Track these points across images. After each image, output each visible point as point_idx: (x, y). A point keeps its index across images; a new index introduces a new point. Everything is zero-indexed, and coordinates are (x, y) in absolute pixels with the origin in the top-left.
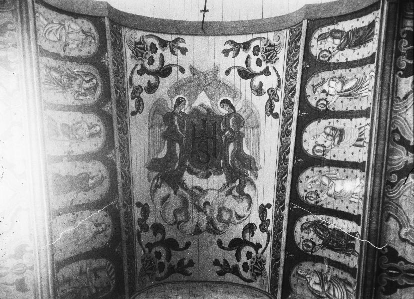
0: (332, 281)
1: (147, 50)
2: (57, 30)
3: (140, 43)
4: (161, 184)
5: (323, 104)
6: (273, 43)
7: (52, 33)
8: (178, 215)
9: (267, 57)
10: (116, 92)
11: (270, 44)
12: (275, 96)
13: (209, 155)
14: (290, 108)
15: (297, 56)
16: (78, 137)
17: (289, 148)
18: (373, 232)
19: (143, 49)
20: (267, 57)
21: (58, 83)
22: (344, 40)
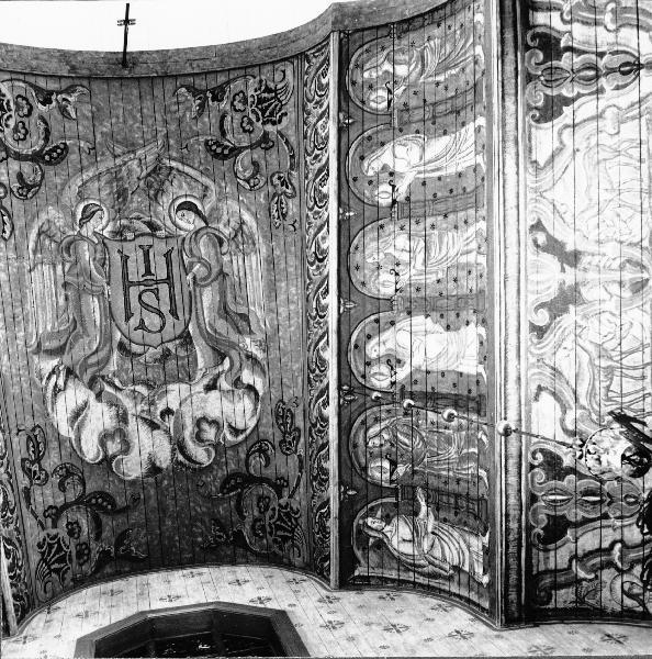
0: (437, 532)
1: (10, 110)
4: (65, 384)
6: (272, 85)
8: (109, 443)
9: (264, 112)
14: (320, 207)
17: (327, 285)
20: (264, 112)
22: (416, 66)
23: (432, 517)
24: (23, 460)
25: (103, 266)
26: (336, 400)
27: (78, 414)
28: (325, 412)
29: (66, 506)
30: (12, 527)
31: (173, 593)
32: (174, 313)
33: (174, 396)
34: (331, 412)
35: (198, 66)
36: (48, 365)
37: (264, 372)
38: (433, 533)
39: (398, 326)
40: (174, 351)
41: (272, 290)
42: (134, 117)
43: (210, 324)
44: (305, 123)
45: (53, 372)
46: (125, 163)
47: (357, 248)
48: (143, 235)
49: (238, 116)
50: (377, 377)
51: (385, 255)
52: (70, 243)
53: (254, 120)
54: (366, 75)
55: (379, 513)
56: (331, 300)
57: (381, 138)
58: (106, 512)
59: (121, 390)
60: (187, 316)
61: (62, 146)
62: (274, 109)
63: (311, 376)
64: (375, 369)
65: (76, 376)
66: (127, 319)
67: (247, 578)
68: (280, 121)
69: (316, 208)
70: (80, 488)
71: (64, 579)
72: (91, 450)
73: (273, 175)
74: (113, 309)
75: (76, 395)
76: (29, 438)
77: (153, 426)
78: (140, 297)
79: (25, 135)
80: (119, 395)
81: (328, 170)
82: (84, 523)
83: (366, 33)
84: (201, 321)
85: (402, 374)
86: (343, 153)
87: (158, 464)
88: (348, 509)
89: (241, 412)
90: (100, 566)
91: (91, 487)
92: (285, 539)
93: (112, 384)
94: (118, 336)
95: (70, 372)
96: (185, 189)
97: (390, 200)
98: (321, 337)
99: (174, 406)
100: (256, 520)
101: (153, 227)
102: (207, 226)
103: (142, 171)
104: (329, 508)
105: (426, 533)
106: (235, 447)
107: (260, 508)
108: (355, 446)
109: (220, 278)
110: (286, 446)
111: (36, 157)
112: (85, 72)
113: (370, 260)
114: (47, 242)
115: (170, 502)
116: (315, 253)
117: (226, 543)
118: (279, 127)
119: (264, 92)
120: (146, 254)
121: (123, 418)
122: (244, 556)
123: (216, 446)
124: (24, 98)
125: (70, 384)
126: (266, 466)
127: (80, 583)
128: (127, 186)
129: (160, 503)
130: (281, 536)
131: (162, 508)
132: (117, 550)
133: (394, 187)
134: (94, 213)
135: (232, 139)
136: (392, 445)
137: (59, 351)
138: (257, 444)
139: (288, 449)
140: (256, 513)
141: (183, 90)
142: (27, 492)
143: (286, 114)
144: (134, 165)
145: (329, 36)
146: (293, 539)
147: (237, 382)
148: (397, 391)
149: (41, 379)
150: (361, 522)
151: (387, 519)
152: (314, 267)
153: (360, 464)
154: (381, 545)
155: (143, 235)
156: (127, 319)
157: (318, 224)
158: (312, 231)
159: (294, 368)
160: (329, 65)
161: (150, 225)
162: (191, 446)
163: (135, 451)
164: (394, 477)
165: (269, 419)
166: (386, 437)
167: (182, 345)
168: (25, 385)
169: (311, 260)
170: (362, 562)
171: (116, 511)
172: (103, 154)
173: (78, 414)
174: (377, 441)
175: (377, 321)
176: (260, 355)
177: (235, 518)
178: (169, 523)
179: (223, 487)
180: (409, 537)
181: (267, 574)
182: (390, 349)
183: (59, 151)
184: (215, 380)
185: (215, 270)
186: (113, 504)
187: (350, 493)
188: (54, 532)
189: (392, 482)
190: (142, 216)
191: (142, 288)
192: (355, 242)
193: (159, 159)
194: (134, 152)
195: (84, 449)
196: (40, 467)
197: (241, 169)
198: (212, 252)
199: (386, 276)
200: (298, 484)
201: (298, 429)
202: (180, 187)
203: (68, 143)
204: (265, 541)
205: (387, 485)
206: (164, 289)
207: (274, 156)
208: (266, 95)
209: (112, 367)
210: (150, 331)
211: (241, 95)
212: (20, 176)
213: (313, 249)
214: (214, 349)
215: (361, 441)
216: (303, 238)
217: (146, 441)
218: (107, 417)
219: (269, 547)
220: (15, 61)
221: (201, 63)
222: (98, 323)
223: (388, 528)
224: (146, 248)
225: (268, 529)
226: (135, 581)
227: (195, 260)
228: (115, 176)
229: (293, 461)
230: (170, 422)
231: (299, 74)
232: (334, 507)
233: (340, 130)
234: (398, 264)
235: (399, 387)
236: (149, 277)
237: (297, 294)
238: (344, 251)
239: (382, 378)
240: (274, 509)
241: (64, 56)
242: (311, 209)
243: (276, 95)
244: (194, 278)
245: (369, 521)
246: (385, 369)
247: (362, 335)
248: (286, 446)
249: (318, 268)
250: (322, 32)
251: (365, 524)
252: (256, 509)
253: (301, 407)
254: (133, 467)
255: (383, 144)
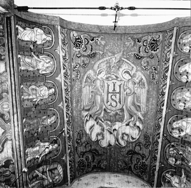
0: (186, 183)
1: (83, 43)
2: (30, 34)
3: (79, 39)
4: (89, 119)
5: (185, 78)
6: (155, 39)
7: (26, 35)
8: (99, 136)
9: (152, 47)
10: (64, 69)
11: (154, 39)
12: (156, 71)
13: (116, 103)
14: (165, 79)
15: (170, 49)
16: (41, 95)
17: (164, 103)
18: (178, 49)
19: (80, 42)
20: (152, 47)
21: (29, 65)
23: (185, 178)
24: (77, 139)
25: (102, 87)
26: (162, 138)
27: (92, 128)
28: (158, 140)
29: (86, 152)
30: (72, 157)
31: (110, 181)
32: (120, 102)
33: (117, 125)
34: (160, 141)
35: (135, 31)
36: (85, 113)
37: (143, 123)
38: (185, 183)
39: (183, 119)
40: (118, 113)
41: (148, 100)
42: (115, 45)
43: (129, 107)
44: (164, 52)
45: (86, 116)
46: (111, 58)
47: (174, 94)
48: (114, 79)
49: (144, 47)
50: (175, 133)
51: (182, 97)
52: (94, 80)
53: (149, 49)
54: (184, 41)
55: (170, 173)
56: (164, 108)
57: (186, 61)
58: (96, 155)
59: (103, 122)
60: (123, 104)
61: (95, 53)
62: (155, 46)
63: (156, 128)
64: (174, 131)
65: (92, 117)
66: (107, 102)
67: (131, 181)
68: (156, 50)
69: (163, 79)
70: (90, 147)
71: (83, 171)
72: (94, 138)
73: (152, 66)
74: (104, 100)
75: (91, 122)
76: (79, 133)
77: (111, 133)
78: (111, 96)
79: (86, 50)
80: (103, 124)
81: (168, 68)
82: (90, 157)
83: (185, 28)
84: (127, 106)
85: (182, 134)
86: (174, 64)
87: (111, 144)
88: (161, 170)
89: (135, 134)
90: (93, 169)
91: (93, 147)
92: (143, 172)
93: (101, 120)
94: (104, 107)
95: (90, 116)
96: (127, 67)
97: (186, 81)
98: (160, 118)
99: (117, 129)
100: (135, 164)
101: (117, 77)
102: (132, 79)
103: (116, 61)
104: (160, 136)
105: (183, 183)
106: (132, 143)
107: (137, 161)
108: (166, 152)
109: (134, 94)
110: (147, 146)
111: (89, 56)
112: (103, 32)
113: (177, 98)
114: (89, 80)
115: (113, 154)
116: (161, 92)
117: (126, 169)
118: (156, 52)
119: (153, 41)
120: (114, 85)
121: (103, 130)
122: (131, 173)
123: (127, 141)
124: (87, 39)
125: (90, 119)
126: (140, 150)
127: (87, 173)
128: (111, 65)
129: (110, 154)
130: (141, 170)
131: (111, 156)
132: (98, 165)
133: (188, 77)
134: (101, 72)
135: (142, 54)
136: (177, 154)
137: (88, 110)
138: (138, 143)
139: (147, 147)
140: (136, 163)
141: (130, 38)
142: (77, 147)
143: (158, 48)
144: (114, 59)
145: (174, 28)
146: (145, 172)
147: (135, 125)
148: (180, 139)
149: (83, 117)
150: (164, 174)
151: (172, 175)
152: (161, 96)
153: (166, 158)
154: (169, 182)
155: (114, 79)
156: (107, 102)
157: (164, 84)
158: (162, 85)
159: (151, 124)
160: (173, 36)
161: (116, 76)
162: (120, 141)
163: (105, 140)
164: (176, 164)
165: (142, 137)
166: (175, 151)
167: (121, 112)
168: (79, 119)
169: (160, 94)
170: (163, 185)
171: (99, 155)
172: (106, 55)
173: (92, 128)
174: (172, 152)
175: (177, 117)
176: (142, 118)
177: (130, 162)
178: (112, 160)
179: (127, 154)
180: (178, 182)
181: (136, 181)
182: (179, 126)
183: (94, 54)
184: (129, 123)
185: (133, 92)
186: (98, 153)
187: (163, 165)
188: (82, 159)
189: (175, 165)
190: (114, 74)
191: (112, 94)
192: (174, 92)
193: (120, 58)
194: (114, 55)
195: (92, 137)
196: (80, 141)
197: (143, 63)
198: (133, 86)
199: (181, 104)
200: (148, 158)
201: (150, 142)
202: (126, 66)
203: (97, 52)
204: (137, 171)
205: (174, 166)
206: (118, 95)
207: (153, 61)
208: (153, 42)
209: (102, 115)
210: (113, 107)
211: (146, 41)
212: (83, 61)
213: (161, 91)
214: (130, 114)
215: (167, 151)
216: (158, 86)
217: (108, 137)
218: (99, 129)
219: (138, 173)
220: (85, 29)
221: (136, 30)
222: (99, 103)
223: (172, 178)
224: (114, 83)
225: (138, 168)
226: (102, 174)
227: (127, 88)
228: (108, 62)
229: (148, 150)
230: (115, 133)
231: (164, 37)
232: (157, 168)
233: (173, 58)
234: (186, 101)
235: (181, 138)
236: (114, 91)
237: (155, 103)
238: (170, 95)
239: (176, 134)
240: (141, 163)
241: (98, 27)
242: (162, 79)
243: (156, 42)
244: (127, 93)
245: (167, 174)
246: (178, 132)
247: (172, 120)
248: (147, 146)
249: (162, 97)
250: (172, 25)
251: (165, 175)
252: (136, 161)
253: (152, 136)
254: (104, 144)
255: (186, 63)
